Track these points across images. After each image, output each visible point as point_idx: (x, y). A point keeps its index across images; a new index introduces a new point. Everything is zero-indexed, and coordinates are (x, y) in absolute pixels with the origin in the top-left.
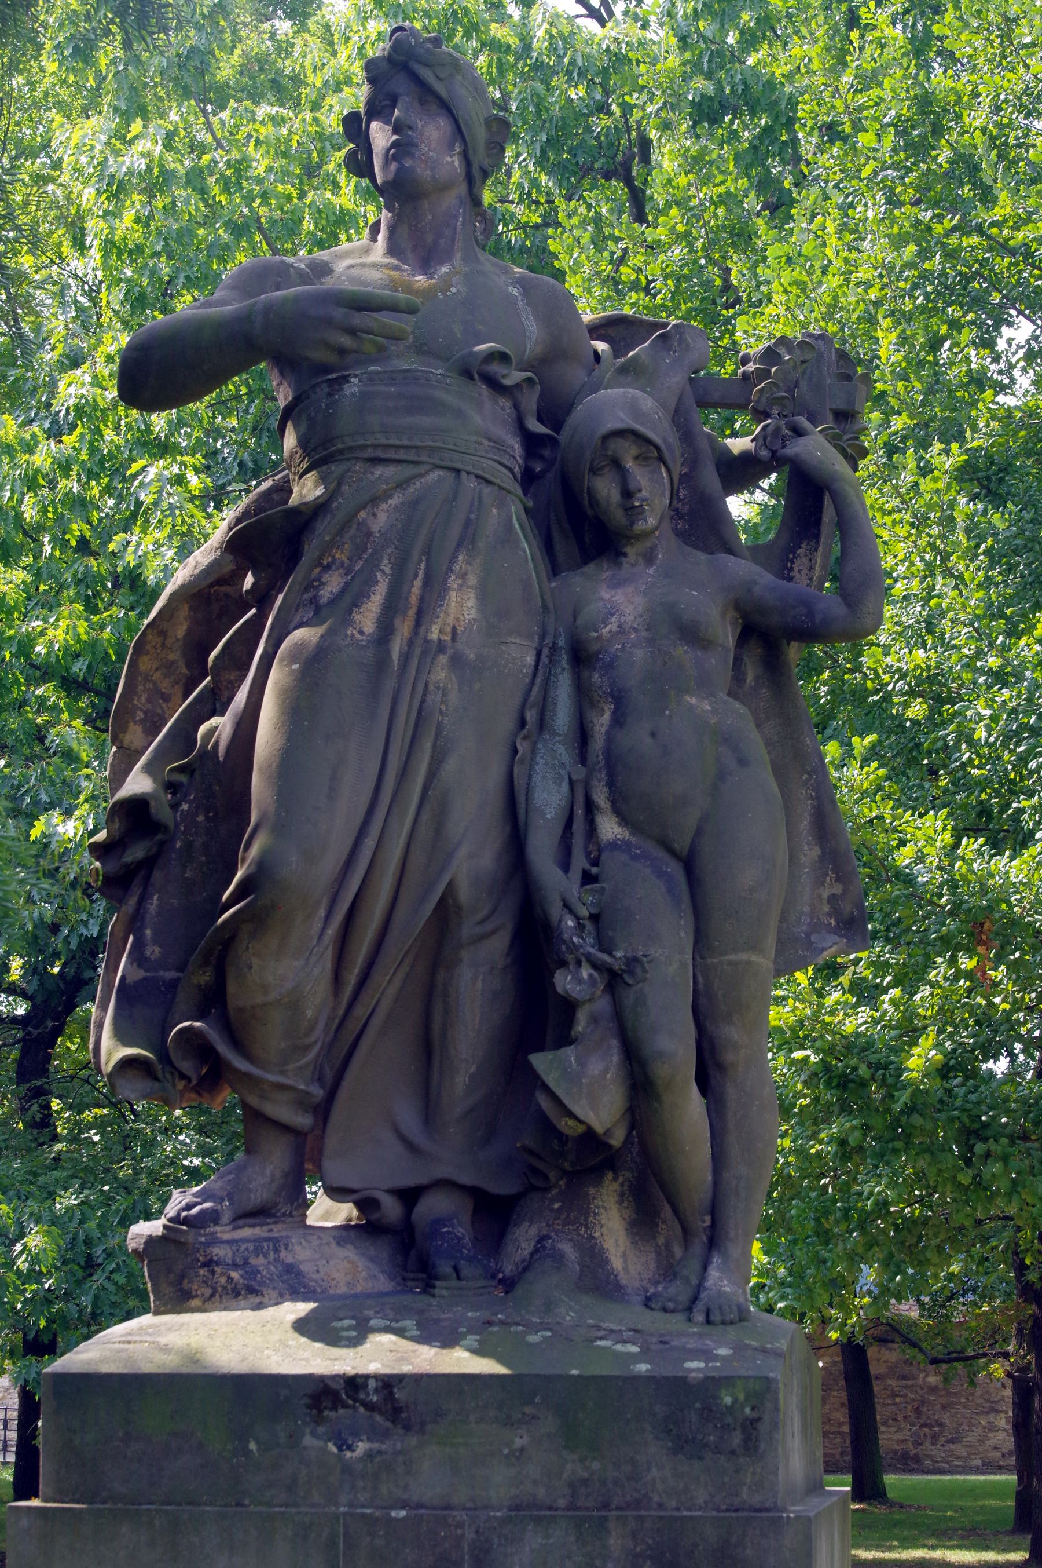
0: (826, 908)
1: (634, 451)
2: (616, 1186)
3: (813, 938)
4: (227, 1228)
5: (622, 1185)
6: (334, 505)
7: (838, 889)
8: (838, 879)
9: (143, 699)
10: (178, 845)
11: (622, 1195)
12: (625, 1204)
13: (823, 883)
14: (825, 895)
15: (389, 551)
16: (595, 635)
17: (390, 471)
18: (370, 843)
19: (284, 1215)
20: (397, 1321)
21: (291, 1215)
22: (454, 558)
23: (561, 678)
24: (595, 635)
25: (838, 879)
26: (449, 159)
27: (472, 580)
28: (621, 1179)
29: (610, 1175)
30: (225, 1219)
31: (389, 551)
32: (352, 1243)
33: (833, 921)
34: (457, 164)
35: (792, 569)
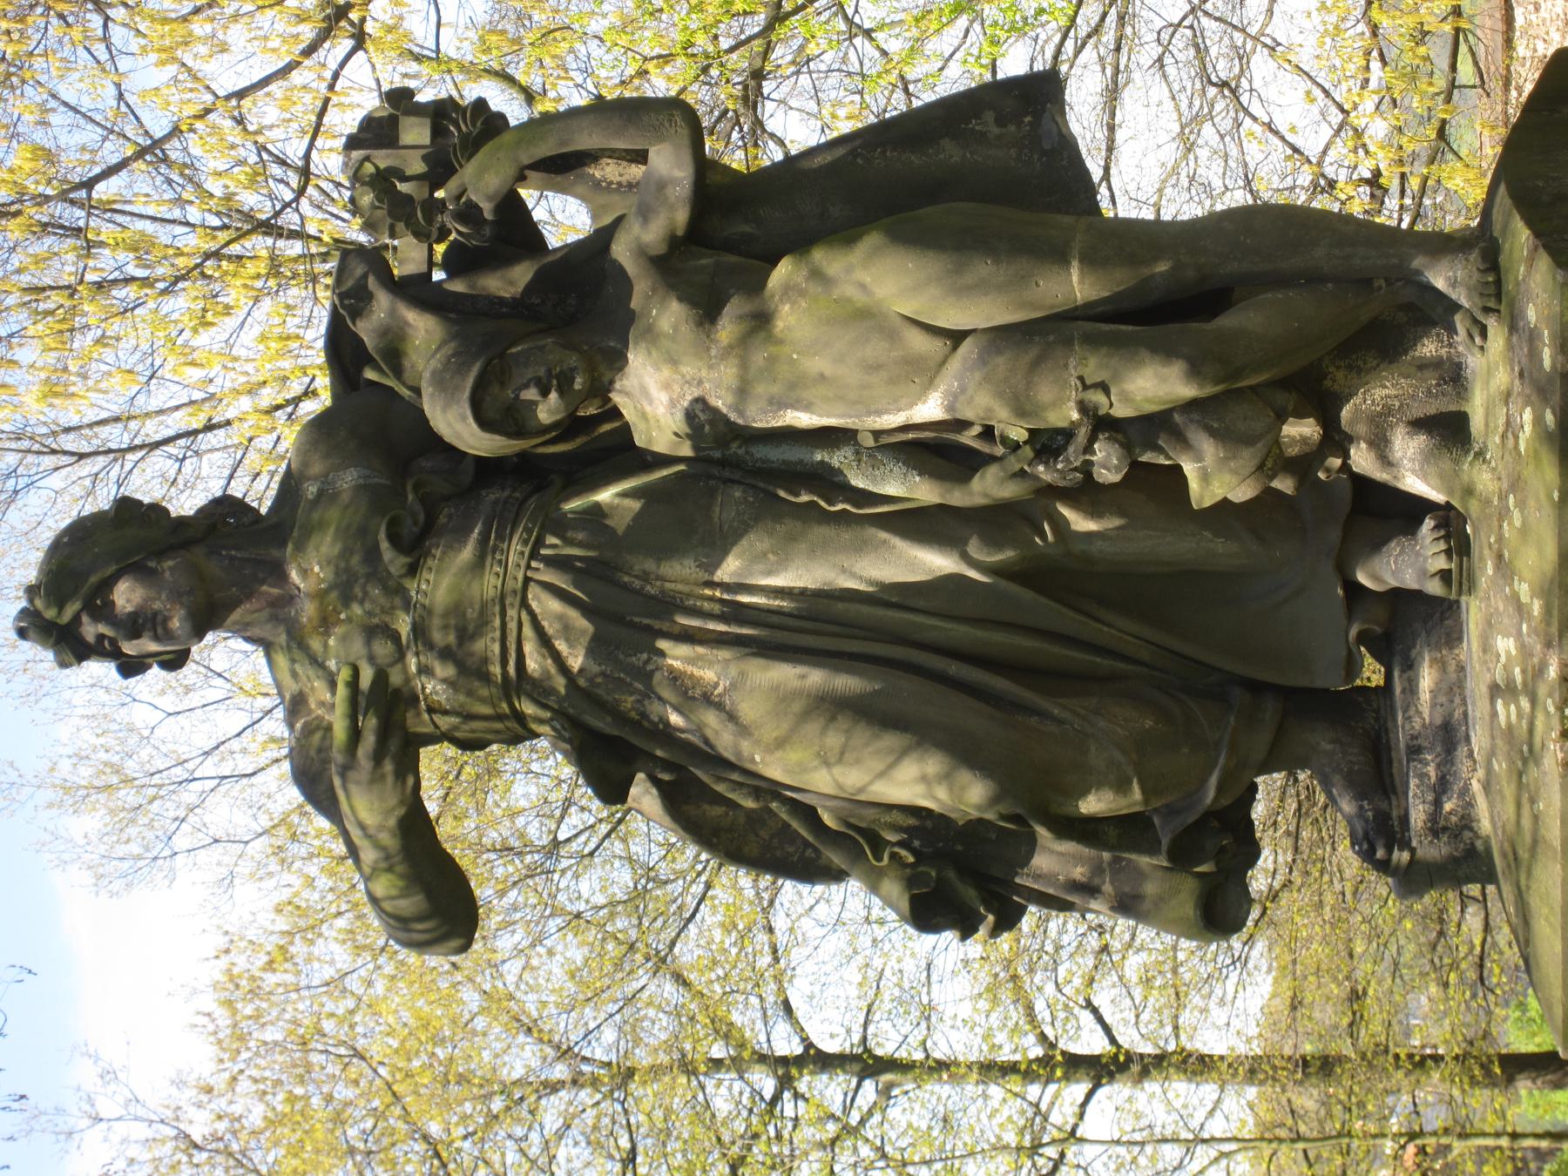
0: (1012, 128)
1: (495, 389)
2: (1340, 375)
3: (1047, 146)
4: (1394, 802)
5: (1338, 368)
6: (571, 711)
7: (989, 116)
8: (977, 116)
9: (791, 850)
10: (959, 848)
11: (1350, 368)
12: (1360, 363)
13: (983, 134)
14: (995, 130)
15: (621, 656)
16: (707, 428)
17: (529, 648)
18: (954, 668)
19: (1377, 719)
20: (1499, 656)
21: (1377, 711)
22: (626, 588)
23: (758, 456)
24: (707, 428)
25: (977, 116)
26: (167, 574)
27: (650, 565)
28: (1331, 369)
29: (1328, 383)
30: (1384, 806)
31: (621, 656)
32: (1410, 649)
33: (1028, 119)
34: (170, 563)
35: (619, 184)
